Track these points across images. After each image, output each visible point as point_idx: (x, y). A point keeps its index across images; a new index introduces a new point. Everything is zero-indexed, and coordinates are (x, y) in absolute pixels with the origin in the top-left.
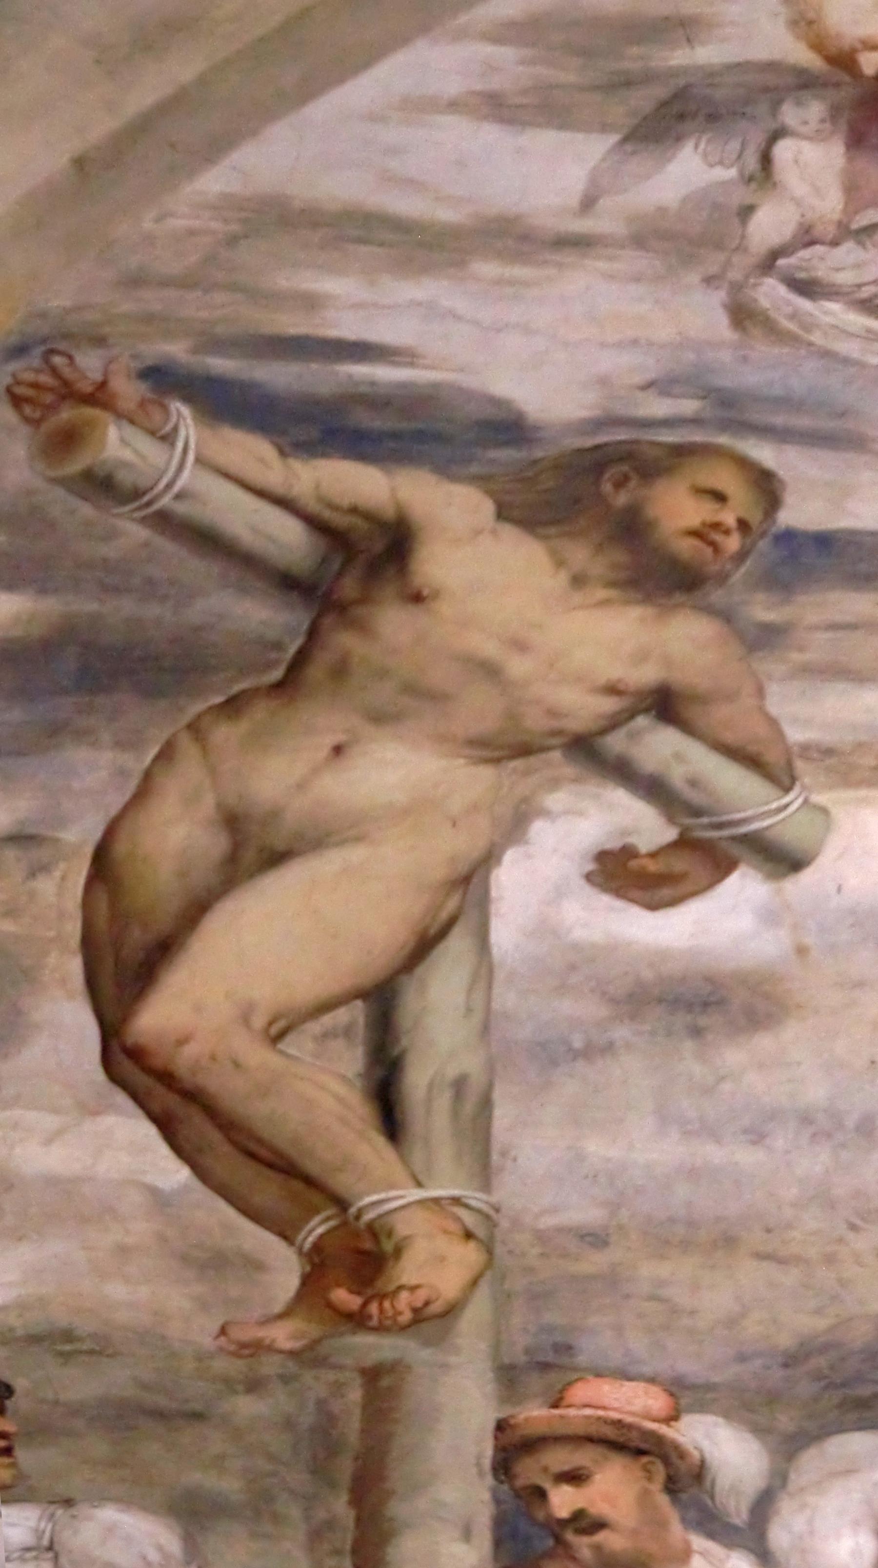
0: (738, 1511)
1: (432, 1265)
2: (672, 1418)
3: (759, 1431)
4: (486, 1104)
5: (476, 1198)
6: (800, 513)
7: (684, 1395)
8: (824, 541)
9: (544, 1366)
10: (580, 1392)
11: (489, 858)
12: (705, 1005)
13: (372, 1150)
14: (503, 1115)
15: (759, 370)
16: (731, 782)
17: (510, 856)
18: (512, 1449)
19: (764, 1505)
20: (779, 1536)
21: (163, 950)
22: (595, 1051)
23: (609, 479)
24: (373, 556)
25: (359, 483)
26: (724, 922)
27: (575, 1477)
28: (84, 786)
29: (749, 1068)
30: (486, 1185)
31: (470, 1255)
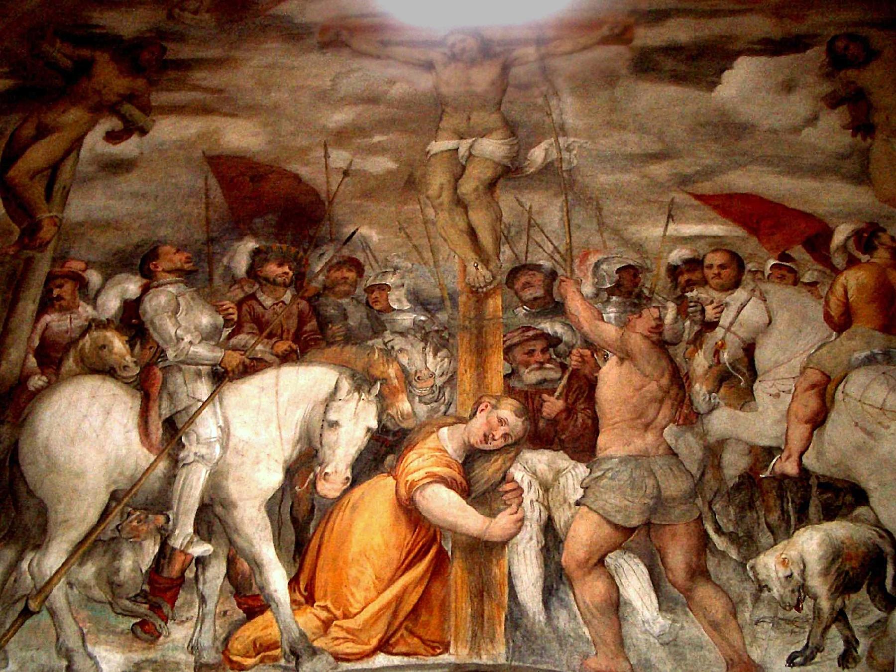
0: (92, 294)
1: (47, 231)
2: (84, 271)
3: (102, 273)
4: (69, 191)
5: (60, 216)
6: (170, 56)
7: (89, 265)
8: (172, 61)
9: (61, 258)
10: (67, 265)
11: (86, 134)
12: (117, 167)
13: (43, 205)
14: (71, 194)
15: (172, 26)
16: (137, 114)
17: (90, 134)
18: (51, 277)
19: (99, 292)
20: (100, 301)
21: (668, 218)
22: (92, 179)
23: (825, 530)
24: (85, 68)
25: (86, 53)
26: (129, 147)
27: (61, 286)
28: (14, 119)
29: (131, 182)
30: (62, 212)
31: (54, 229)
